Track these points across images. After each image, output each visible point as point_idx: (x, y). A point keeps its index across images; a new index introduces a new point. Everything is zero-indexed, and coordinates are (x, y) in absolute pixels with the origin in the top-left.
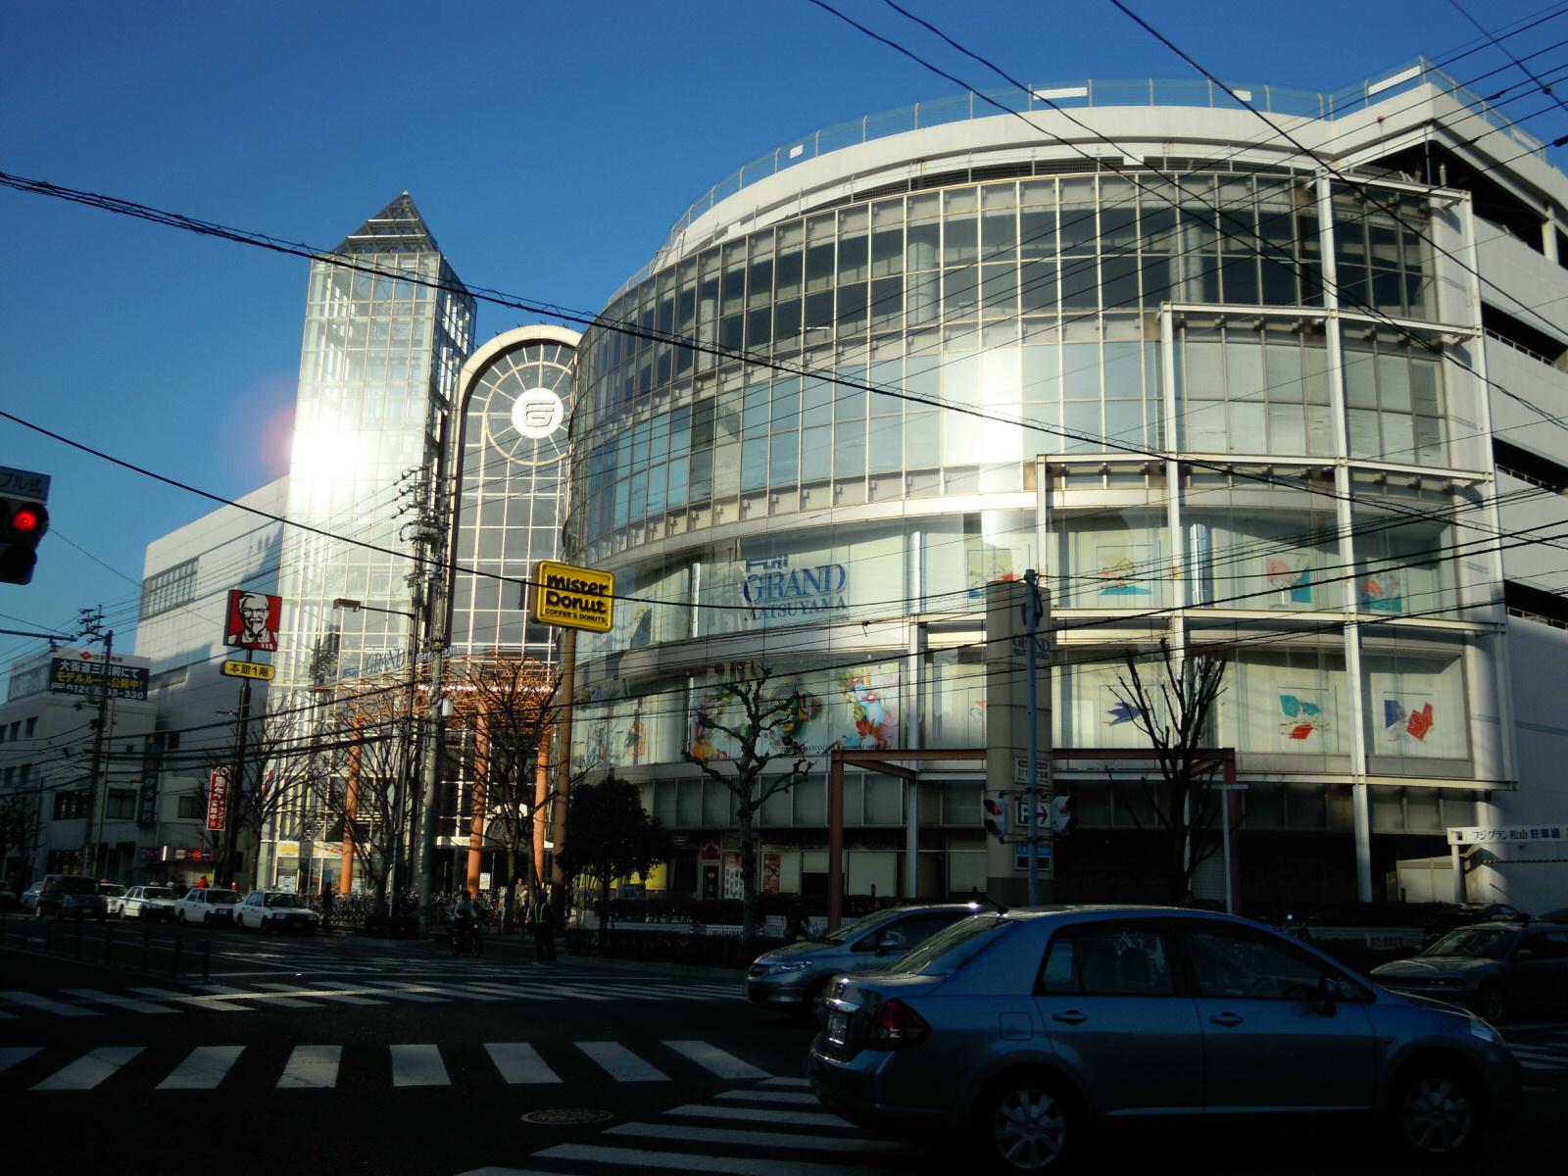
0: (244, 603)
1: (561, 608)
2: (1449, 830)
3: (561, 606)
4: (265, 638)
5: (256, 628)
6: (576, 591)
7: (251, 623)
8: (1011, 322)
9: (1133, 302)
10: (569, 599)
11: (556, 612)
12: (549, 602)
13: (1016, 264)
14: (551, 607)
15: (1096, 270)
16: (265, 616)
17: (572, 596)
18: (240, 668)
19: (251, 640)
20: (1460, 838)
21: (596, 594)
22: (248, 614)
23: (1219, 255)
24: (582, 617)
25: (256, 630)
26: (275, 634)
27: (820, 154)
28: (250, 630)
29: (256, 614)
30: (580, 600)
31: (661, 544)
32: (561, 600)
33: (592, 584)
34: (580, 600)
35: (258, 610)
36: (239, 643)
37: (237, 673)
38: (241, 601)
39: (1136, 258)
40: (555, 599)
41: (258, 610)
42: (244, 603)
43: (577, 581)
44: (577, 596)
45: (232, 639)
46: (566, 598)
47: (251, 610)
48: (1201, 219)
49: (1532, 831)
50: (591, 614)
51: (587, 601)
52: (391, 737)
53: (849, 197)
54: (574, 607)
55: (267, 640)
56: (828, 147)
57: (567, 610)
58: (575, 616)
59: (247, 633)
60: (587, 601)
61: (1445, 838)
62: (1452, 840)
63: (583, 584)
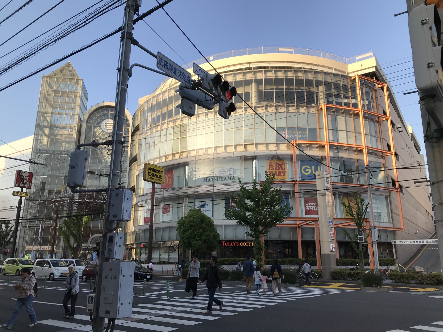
0: (21, 174)
1: (151, 177)
2: (392, 241)
3: (151, 176)
4: (27, 185)
5: (25, 182)
6: (155, 172)
7: (23, 180)
8: (294, 106)
9: (294, 103)
10: (152, 176)
11: (150, 178)
12: (149, 175)
13: (294, 91)
14: (149, 176)
15: (294, 94)
16: (28, 178)
17: (154, 173)
18: (19, 193)
19: (23, 185)
20: (395, 243)
21: (160, 173)
22: (22, 177)
23: (264, 91)
24: (157, 179)
25: (25, 182)
26: (31, 184)
27: (219, 59)
28: (23, 182)
29: (25, 178)
30: (156, 175)
31: (164, 163)
32: (152, 174)
33: (159, 170)
34: (156, 175)
35: (25, 176)
36: (19, 186)
37: (18, 195)
38: (20, 173)
39: (263, 91)
40: (150, 174)
41: (25, 176)
42: (21, 174)
43: (155, 169)
44: (156, 173)
45: (17, 184)
46: (153, 174)
47: (24, 176)
48: (258, 82)
49: (416, 241)
50: (159, 179)
51: (158, 175)
52: (22, 220)
53: (235, 70)
54: (155, 177)
55: (28, 185)
56: (221, 57)
57: (153, 177)
58: (155, 179)
59: (22, 183)
60: (158, 175)
61: (391, 243)
62: (393, 243)
63: (157, 170)
